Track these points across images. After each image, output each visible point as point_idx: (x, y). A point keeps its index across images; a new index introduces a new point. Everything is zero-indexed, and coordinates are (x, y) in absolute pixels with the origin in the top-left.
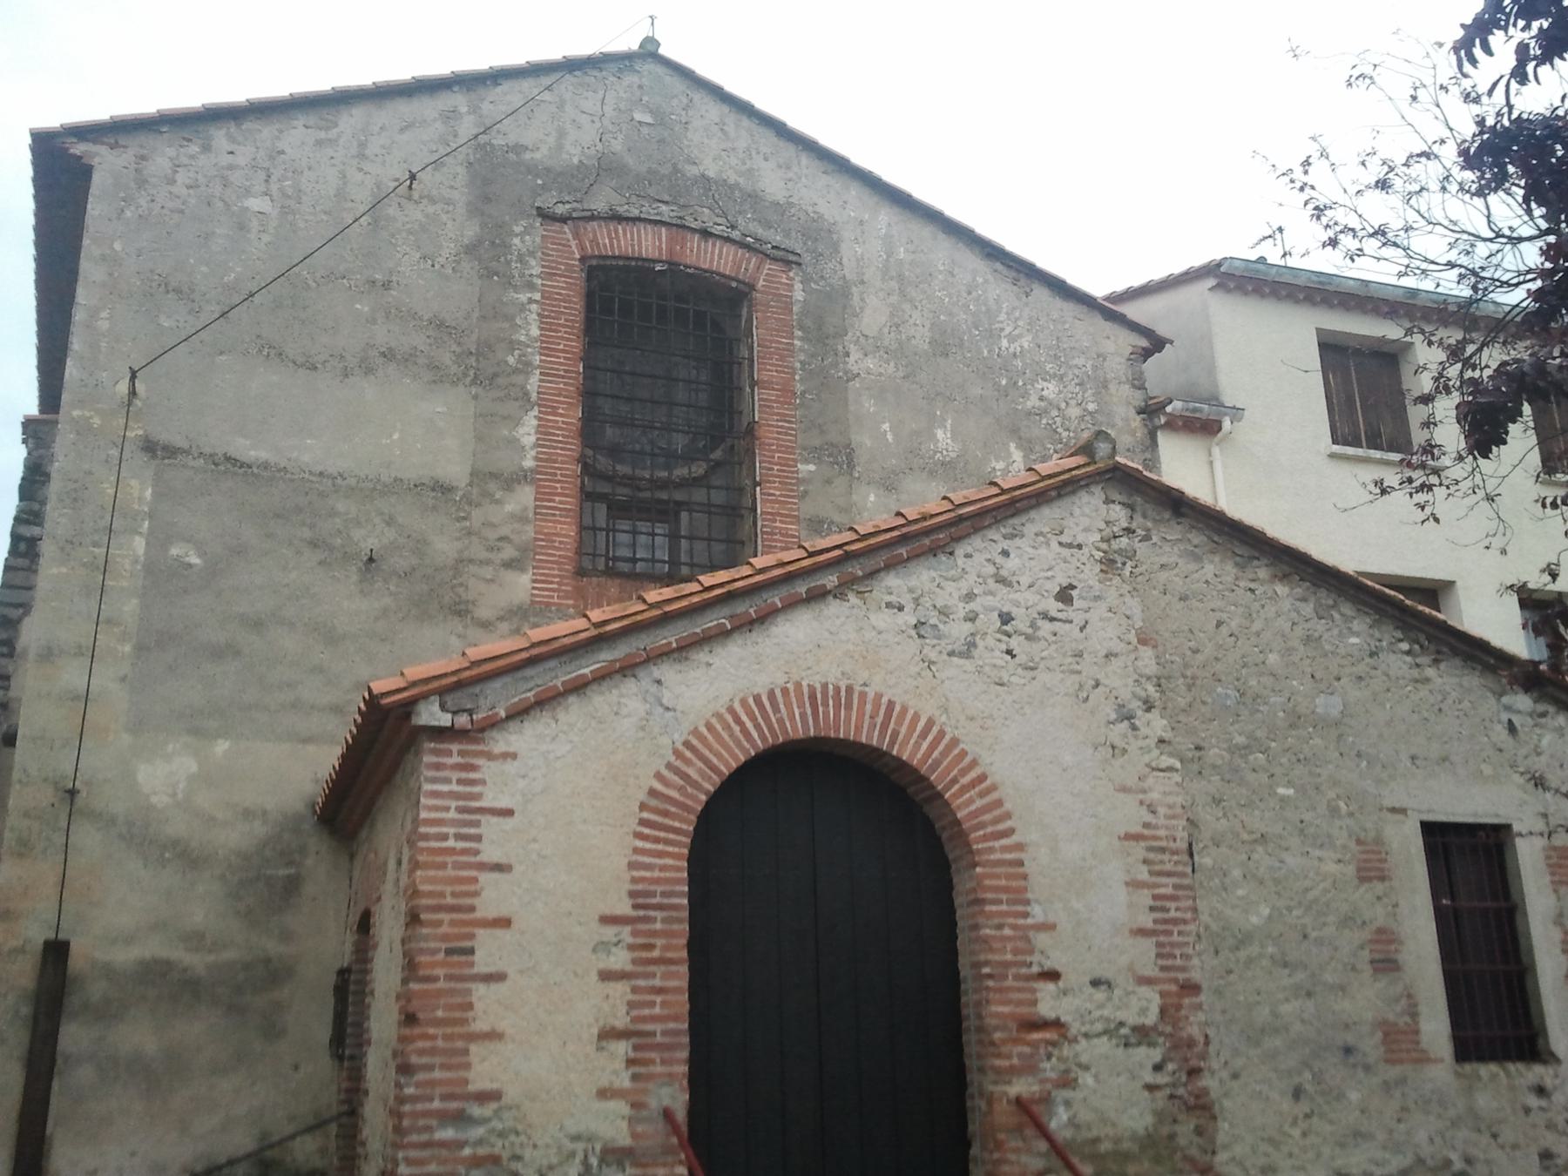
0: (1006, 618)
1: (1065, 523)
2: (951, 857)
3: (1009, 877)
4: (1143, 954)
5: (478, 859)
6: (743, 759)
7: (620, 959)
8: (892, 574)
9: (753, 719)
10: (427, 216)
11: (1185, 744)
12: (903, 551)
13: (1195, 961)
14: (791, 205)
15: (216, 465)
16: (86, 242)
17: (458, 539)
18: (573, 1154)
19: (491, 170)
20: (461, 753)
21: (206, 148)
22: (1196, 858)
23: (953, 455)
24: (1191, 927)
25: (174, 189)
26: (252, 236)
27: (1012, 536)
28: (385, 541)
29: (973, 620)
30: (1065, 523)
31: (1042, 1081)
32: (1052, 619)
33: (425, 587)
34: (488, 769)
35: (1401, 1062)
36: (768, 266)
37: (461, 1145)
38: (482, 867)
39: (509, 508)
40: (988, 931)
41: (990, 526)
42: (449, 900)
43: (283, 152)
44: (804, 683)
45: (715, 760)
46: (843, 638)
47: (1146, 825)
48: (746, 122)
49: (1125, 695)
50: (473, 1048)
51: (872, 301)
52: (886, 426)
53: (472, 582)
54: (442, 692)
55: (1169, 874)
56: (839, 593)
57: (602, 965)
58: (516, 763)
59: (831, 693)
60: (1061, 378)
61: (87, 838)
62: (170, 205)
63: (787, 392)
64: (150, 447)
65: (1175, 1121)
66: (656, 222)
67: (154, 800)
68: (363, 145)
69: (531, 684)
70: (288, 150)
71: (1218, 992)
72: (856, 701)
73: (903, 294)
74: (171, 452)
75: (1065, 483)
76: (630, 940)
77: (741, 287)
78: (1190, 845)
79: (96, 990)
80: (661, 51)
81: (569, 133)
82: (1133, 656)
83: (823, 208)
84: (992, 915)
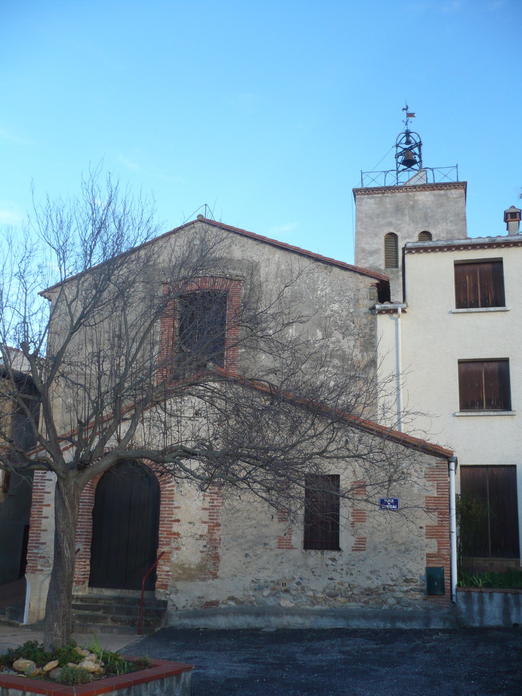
13: (221, 517)
14: (243, 259)
31: (171, 548)
35: (283, 548)
37: (38, 553)
42: (38, 500)
71: (226, 526)
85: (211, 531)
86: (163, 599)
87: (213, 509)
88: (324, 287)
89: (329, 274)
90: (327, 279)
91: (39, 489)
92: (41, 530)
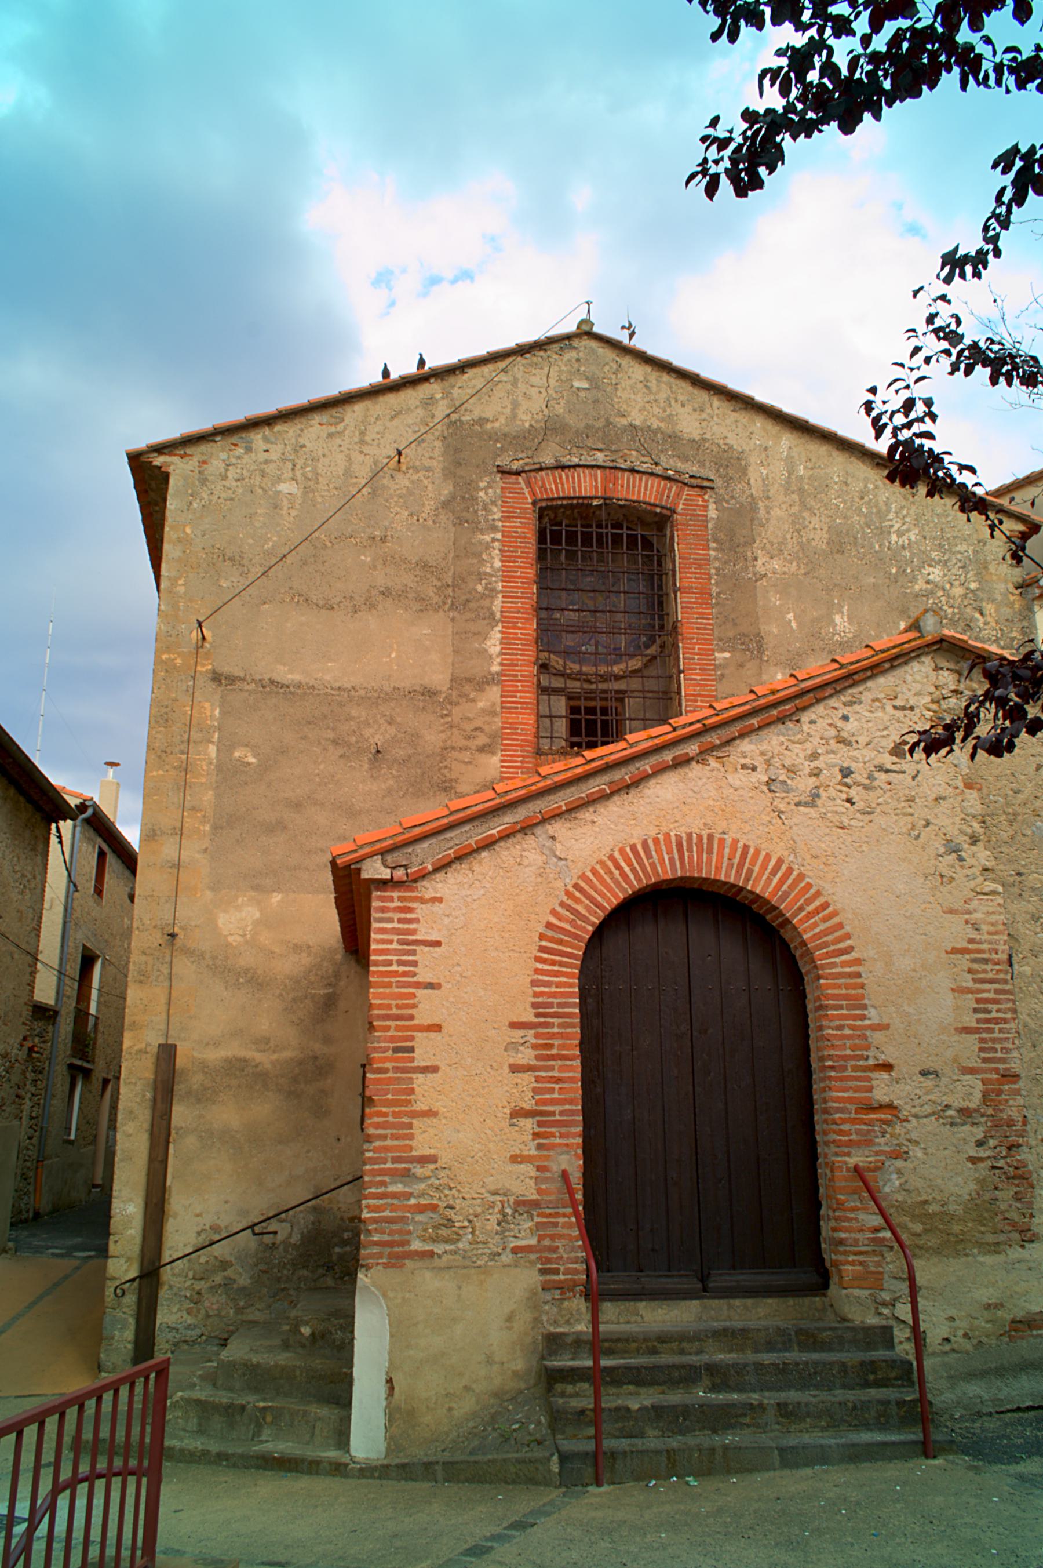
0: (846, 772)
1: (898, 689)
2: (803, 971)
3: (847, 987)
4: (969, 1048)
5: (415, 979)
6: (622, 896)
7: (526, 1056)
8: (746, 741)
9: (630, 864)
10: (413, 482)
11: (1007, 871)
12: (754, 721)
13: (1015, 1054)
14: (705, 440)
15: (263, 687)
16: (167, 529)
17: (442, 732)
18: (492, 1206)
19: (461, 440)
20: (400, 899)
21: (249, 450)
22: (1016, 967)
23: (850, 635)
24: (1012, 1025)
25: (227, 483)
26: (284, 512)
27: (851, 704)
28: (388, 736)
29: (817, 775)
30: (898, 689)
31: (877, 1153)
32: (887, 771)
33: (419, 771)
34: (421, 910)
36: (687, 491)
37: (409, 1195)
38: (418, 985)
39: (481, 705)
40: (830, 1031)
41: (831, 696)
42: (395, 1011)
43: (304, 446)
44: (672, 834)
45: (599, 899)
46: (705, 795)
47: (971, 941)
48: (665, 377)
49: (953, 831)
50: (415, 1122)
51: (776, 512)
52: (790, 616)
53: (455, 765)
54: (383, 853)
55: (991, 981)
56: (700, 758)
57: (512, 1061)
58: (442, 905)
59: (695, 840)
60: (946, 562)
61: (184, 967)
62: (223, 495)
63: (705, 593)
64: (217, 677)
65: (996, 1188)
66: (592, 467)
67: (230, 939)
68: (363, 433)
69: (452, 844)
70: (308, 444)
71: (1035, 1079)
72: (715, 846)
73: (802, 503)
74: (232, 680)
75: (897, 657)
76: (534, 1041)
77: (665, 512)
78: (1010, 956)
79: (197, 1080)
80: (595, 329)
81: (524, 401)
82: (960, 799)
83: (732, 441)
84: (832, 1018)
85: (993, 1096)
86: (872, 1320)
87: (991, 1031)
88: (905, 527)
89: (911, 499)
90: (909, 509)
91: (395, 974)
92: (415, 1115)
